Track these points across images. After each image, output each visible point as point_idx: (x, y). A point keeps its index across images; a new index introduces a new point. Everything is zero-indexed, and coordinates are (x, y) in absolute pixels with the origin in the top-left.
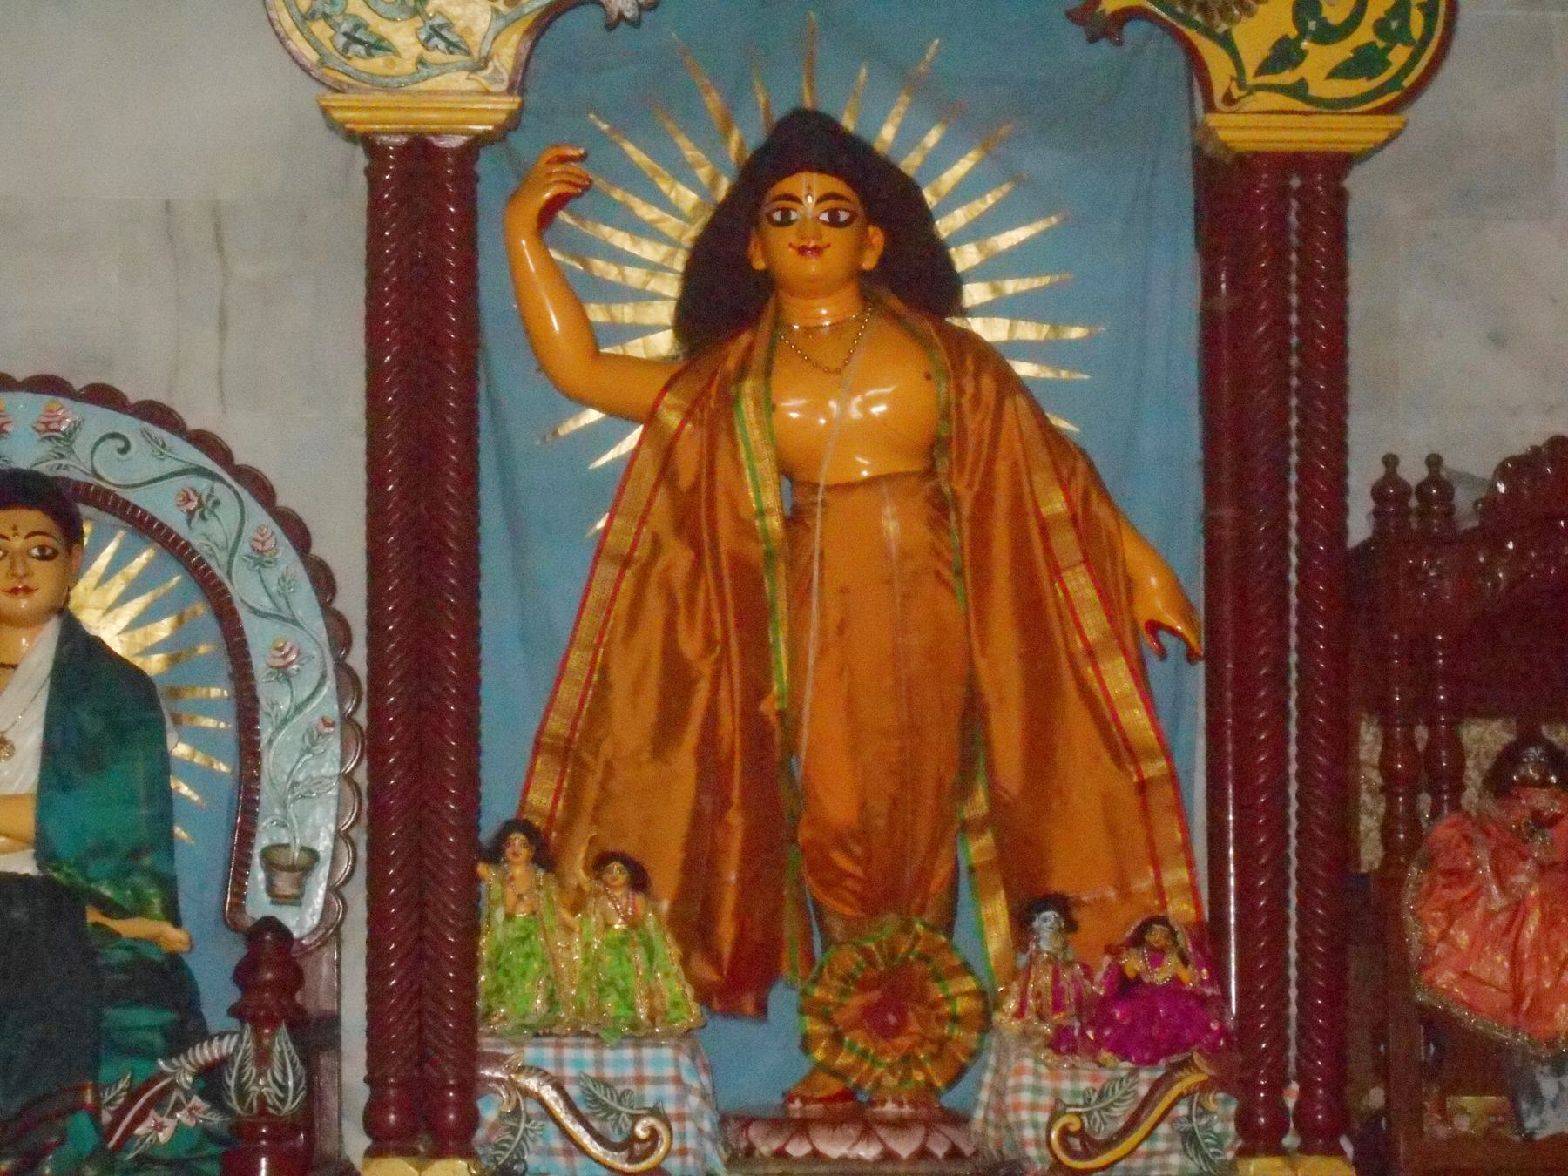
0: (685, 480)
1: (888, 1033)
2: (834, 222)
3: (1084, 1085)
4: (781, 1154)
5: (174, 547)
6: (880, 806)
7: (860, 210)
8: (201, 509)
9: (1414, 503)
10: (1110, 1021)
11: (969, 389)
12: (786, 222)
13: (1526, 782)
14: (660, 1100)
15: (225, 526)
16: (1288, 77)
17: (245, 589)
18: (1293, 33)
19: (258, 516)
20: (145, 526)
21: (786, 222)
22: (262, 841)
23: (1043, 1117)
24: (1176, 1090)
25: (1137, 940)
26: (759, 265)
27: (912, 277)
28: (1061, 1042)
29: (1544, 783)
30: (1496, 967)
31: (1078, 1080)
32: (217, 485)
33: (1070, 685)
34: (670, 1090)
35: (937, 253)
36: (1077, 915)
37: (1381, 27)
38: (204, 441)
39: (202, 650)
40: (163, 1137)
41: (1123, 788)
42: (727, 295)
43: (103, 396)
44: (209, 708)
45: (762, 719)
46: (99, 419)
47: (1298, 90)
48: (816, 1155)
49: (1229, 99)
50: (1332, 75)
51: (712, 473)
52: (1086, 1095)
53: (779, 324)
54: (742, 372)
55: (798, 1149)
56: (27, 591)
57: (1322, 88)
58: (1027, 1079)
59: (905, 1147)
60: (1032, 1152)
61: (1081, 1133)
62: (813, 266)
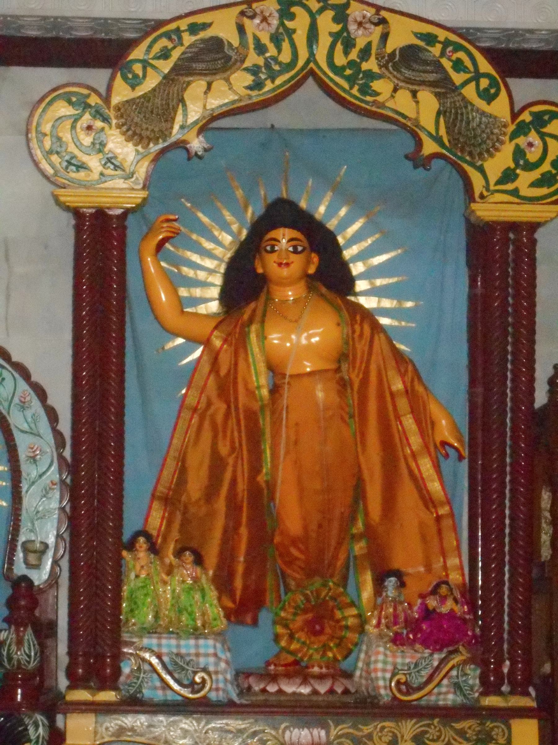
0: (223, 372)
2: (295, 252)
3: (407, 660)
4: (264, 691)
6: (313, 526)
7: (306, 243)
10: (421, 630)
12: (273, 251)
16: (510, 187)
18: (513, 166)
19: (23, 385)
21: (273, 251)
22: (22, 538)
23: (388, 675)
25: (434, 591)
27: (332, 278)
31: (405, 658)
34: (212, 660)
35: (344, 266)
36: (405, 579)
41: (429, 518)
42: (244, 285)
47: (515, 193)
49: (482, 197)
51: (236, 364)
53: (269, 299)
55: (272, 688)
57: (525, 191)
58: (381, 657)
59: (323, 688)
60: (382, 692)
61: (406, 683)
62: (285, 272)
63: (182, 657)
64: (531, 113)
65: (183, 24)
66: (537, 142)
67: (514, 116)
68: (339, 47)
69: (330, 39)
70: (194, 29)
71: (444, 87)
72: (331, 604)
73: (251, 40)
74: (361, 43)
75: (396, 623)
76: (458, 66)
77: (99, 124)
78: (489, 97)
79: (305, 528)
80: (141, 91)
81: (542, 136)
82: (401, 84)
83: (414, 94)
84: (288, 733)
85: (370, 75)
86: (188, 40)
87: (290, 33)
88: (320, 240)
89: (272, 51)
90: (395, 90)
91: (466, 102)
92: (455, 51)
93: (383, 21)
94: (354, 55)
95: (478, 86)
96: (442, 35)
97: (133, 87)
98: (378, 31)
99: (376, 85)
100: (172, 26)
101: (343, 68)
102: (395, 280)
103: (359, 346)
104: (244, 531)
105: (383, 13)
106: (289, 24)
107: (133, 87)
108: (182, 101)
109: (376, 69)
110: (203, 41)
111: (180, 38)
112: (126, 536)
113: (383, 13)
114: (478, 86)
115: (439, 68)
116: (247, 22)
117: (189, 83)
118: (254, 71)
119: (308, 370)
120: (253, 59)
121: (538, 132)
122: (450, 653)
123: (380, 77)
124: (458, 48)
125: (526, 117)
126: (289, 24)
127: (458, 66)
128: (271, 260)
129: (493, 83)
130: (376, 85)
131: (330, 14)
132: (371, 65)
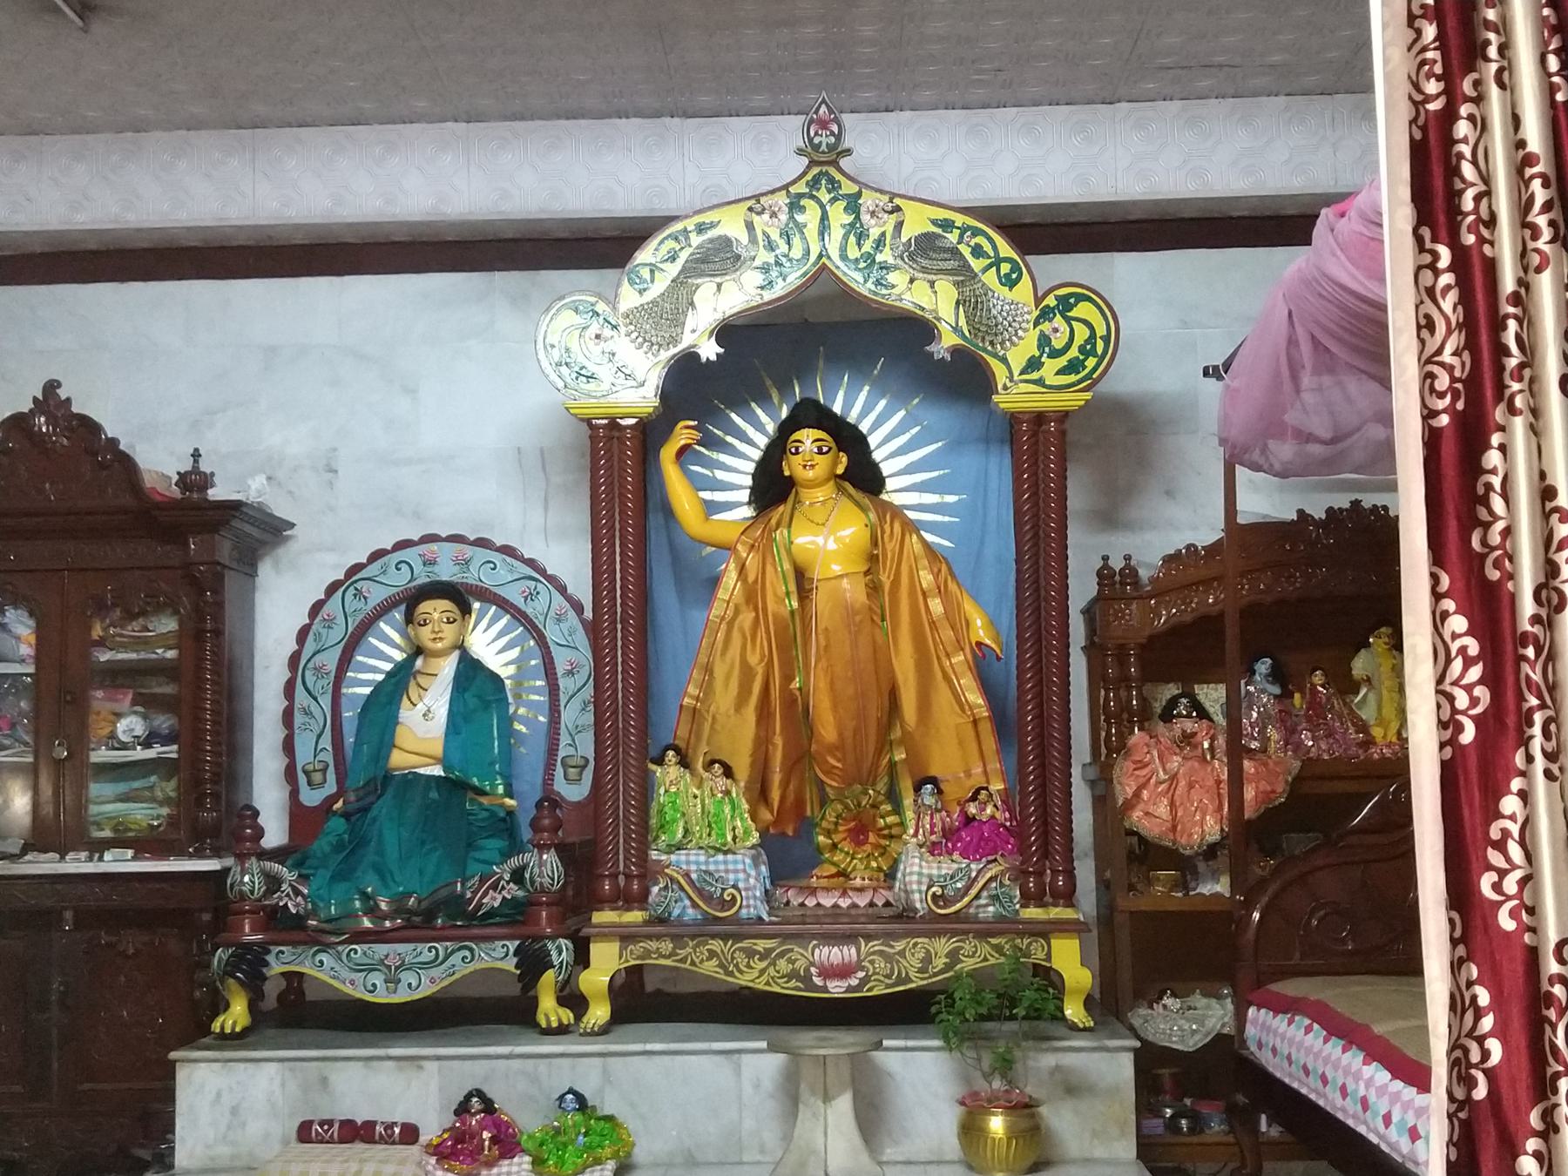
0: (751, 579)
1: (859, 843)
2: (820, 452)
3: (944, 872)
4: (802, 905)
5: (519, 616)
6: (849, 734)
7: (833, 445)
8: (530, 596)
9: (1117, 578)
10: (960, 839)
11: (887, 527)
12: (797, 453)
13: (1180, 715)
14: (737, 881)
15: (543, 605)
16: (1035, 376)
17: (552, 634)
18: (1037, 354)
19: (558, 598)
20: (504, 605)
21: (797, 453)
22: (561, 754)
23: (924, 888)
24: (988, 875)
25: (974, 798)
26: (787, 473)
27: (863, 477)
28: (933, 849)
29: (1189, 716)
30: (1163, 810)
31: (945, 867)
32: (540, 586)
33: (939, 675)
34: (741, 876)
35: (875, 468)
36: (942, 786)
37: (1082, 349)
38: (531, 563)
39: (533, 662)
40: (496, 905)
41: (965, 721)
42: (772, 487)
43: (482, 543)
44: (536, 691)
45: (791, 693)
46: (482, 554)
47: (1040, 382)
48: (818, 905)
49: (1005, 388)
50: (1058, 373)
51: (764, 573)
52: (945, 877)
53: (797, 501)
54: (778, 525)
55: (811, 902)
56: (441, 639)
57: (1052, 380)
58: (916, 869)
59: (862, 901)
60: (918, 905)
61: (942, 896)
62: (810, 474)
63: (711, 874)
64: (1057, 298)
65: (690, 224)
66: (1064, 327)
67: (1038, 300)
68: (852, 239)
69: (842, 232)
70: (701, 229)
71: (963, 275)
72: (872, 811)
73: (760, 237)
74: (875, 233)
75: (932, 833)
76: (978, 251)
77: (607, 332)
78: (1010, 282)
79: (840, 735)
80: (649, 296)
81: (1068, 320)
82: (917, 275)
83: (932, 284)
84: (817, 951)
85: (884, 267)
86: (696, 240)
87: (801, 228)
88: (848, 439)
89: (783, 247)
90: (912, 281)
91: (987, 290)
92: (974, 235)
93: (898, 209)
94: (868, 246)
95: (998, 270)
96: (960, 219)
97: (641, 292)
98: (892, 220)
99: (893, 277)
100: (678, 226)
101: (857, 260)
102: (935, 474)
103: (889, 547)
104: (779, 741)
105: (897, 201)
106: (800, 218)
107: (641, 292)
108: (692, 304)
109: (891, 261)
110: (711, 241)
111: (687, 238)
112: (654, 752)
113: (897, 201)
114: (998, 270)
115: (955, 252)
116: (756, 219)
117: (698, 286)
118: (765, 269)
119: (532, 643)
120: (764, 256)
121: (1064, 317)
122: (989, 862)
123: (896, 268)
124: (976, 232)
125: (1051, 301)
126: (800, 218)
127: (978, 251)
128: (796, 461)
129: (1015, 267)
130: (893, 277)
131: (842, 204)
132: (885, 256)
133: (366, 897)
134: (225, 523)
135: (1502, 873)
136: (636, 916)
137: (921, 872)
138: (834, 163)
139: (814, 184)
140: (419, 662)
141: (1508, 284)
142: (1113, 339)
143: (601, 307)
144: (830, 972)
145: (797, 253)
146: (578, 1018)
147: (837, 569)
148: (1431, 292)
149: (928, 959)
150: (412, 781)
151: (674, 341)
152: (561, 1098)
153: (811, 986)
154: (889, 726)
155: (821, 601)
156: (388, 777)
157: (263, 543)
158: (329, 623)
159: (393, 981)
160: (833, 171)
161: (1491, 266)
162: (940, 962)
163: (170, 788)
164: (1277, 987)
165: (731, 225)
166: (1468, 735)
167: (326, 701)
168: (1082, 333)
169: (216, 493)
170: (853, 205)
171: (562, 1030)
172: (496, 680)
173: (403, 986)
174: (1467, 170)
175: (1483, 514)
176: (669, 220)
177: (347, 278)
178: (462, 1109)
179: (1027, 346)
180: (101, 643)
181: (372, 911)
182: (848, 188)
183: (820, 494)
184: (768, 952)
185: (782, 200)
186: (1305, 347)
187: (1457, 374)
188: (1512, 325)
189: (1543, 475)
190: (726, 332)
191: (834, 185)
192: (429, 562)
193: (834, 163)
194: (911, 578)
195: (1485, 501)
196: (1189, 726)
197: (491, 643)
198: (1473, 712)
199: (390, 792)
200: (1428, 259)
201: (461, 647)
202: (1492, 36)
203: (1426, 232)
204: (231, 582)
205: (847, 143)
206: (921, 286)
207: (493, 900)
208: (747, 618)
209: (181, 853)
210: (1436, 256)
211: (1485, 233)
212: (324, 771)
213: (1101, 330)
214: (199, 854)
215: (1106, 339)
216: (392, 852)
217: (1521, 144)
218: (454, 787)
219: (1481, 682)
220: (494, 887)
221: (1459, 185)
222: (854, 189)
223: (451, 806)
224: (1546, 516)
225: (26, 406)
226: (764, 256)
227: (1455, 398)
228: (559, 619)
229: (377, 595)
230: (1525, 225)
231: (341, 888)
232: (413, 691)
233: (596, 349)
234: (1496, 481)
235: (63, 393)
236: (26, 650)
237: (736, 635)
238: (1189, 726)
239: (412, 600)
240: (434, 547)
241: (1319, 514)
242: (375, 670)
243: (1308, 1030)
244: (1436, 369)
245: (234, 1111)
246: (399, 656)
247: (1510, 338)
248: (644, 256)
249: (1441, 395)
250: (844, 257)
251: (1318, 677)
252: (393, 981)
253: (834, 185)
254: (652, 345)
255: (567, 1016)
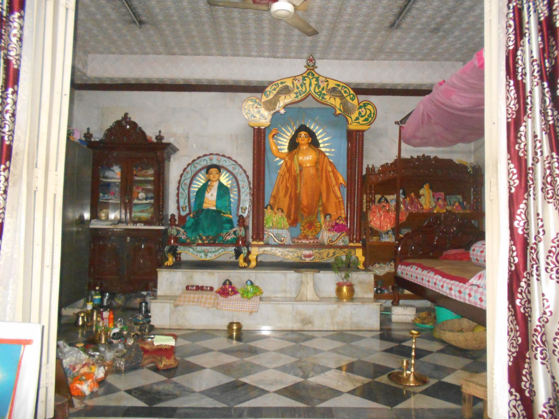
5: (231, 173)
8: (234, 169)
15: (237, 171)
16: (357, 121)
17: (239, 178)
19: (241, 170)
20: (228, 171)
22: (241, 206)
25: (338, 219)
27: (314, 143)
28: (329, 230)
30: (378, 223)
31: (331, 234)
35: (317, 141)
37: (368, 116)
38: (234, 161)
42: (294, 145)
43: (223, 156)
46: (223, 158)
47: (359, 123)
53: (299, 149)
55: (300, 241)
59: (312, 241)
65: (279, 82)
67: (359, 104)
68: (317, 87)
70: (282, 83)
71: (342, 97)
74: (322, 87)
76: (345, 92)
77: (259, 106)
78: (353, 100)
79: (308, 204)
80: (269, 98)
81: (365, 109)
85: (324, 94)
86: (280, 86)
87: (305, 84)
88: (312, 134)
89: (300, 88)
91: (347, 101)
93: (327, 81)
94: (320, 89)
96: (342, 84)
98: (326, 83)
99: (325, 97)
115: (340, 92)
116: (294, 81)
118: (296, 93)
120: (296, 90)
124: (345, 87)
125: (362, 104)
127: (345, 92)
129: (354, 96)
130: (325, 97)
131: (315, 79)
132: (324, 92)
133: (200, 236)
134: (166, 148)
135: (520, 221)
136: (261, 243)
137: (326, 236)
138: (313, 70)
139: (308, 74)
140: (209, 183)
141: (528, 89)
142: (375, 114)
143: (257, 101)
144: (306, 256)
145: (304, 90)
146: (249, 265)
147: (309, 165)
148: (508, 91)
149: (328, 254)
150: (208, 210)
151: (274, 109)
152: (247, 282)
153: (302, 259)
154: (319, 200)
155: (305, 172)
156: (203, 210)
157: (172, 154)
158: (188, 173)
159: (206, 255)
160: (313, 71)
161: (524, 85)
162: (331, 255)
163: (152, 210)
164: (405, 261)
165: (289, 83)
166: (513, 190)
167: (187, 192)
168: (368, 112)
169: (164, 141)
170: (317, 80)
171: (245, 268)
172: (226, 187)
173: (208, 256)
174: (520, 62)
175: (519, 141)
176: (273, 82)
177: (192, 93)
178: (225, 284)
179: (356, 115)
180: (136, 175)
181: (201, 239)
182: (316, 76)
183: (304, 147)
184: (292, 251)
185: (301, 78)
186: (426, 116)
187: (514, 109)
188: (529, 98)
189: (534, 132)
190: (285, 107)
191: (313, 75)
192: (211, 160)
193: (313, 70)
194: (326, 167)
195: (520, 138)
196: (384, 204)
197: (225, 179)
198: (515, 185)
199: (204, 212)
200: (508, 83)
201: (219, 180)
202: (527, 31)
203: (508, 77)
204: (166, 162)
205: (316, 65)
206: (332, 99)
207: (229, 238)
208: (287, 175)
209: (154, 224)
210: (510, 83)
211: (524, 77)
212: (186, 207)
213: (373, 112)
214: (159, 225)
215: (374, 114)
216: (205, 225)
217: (532, 57)
218: (218, 212)
219: (517, 179)
220: (229, 235)
221: (517, 66)
222: (317, 76)
223: (216, 217)
224: (535, 142)
225: (120, 119)
226: (296, 90)
227: (513, 114)
228: (241, 174)
229: (199, 167)
230: (533, 76)
231: (194, 234)
232: (208, 189)
233: (256, 110)
234: (523, 133)
235: (129, 116)
236: (118, 176)
237: (285, 179)
238: (384, 204)
239: (208, 168)
240: (212, 156)
241: (415, 157)
242: (198, 185)
243: (417, 269)
244: (509, 108)
245: (171, 283)
246: (204, 182)
247: (529, 101)
248: (268, 89)
249: (509, 114)
250: (315, 92)
251: (412, 194)
252: (206, 255)
253: (313, 75)
254: (268, 109)
255: (246, 265)
